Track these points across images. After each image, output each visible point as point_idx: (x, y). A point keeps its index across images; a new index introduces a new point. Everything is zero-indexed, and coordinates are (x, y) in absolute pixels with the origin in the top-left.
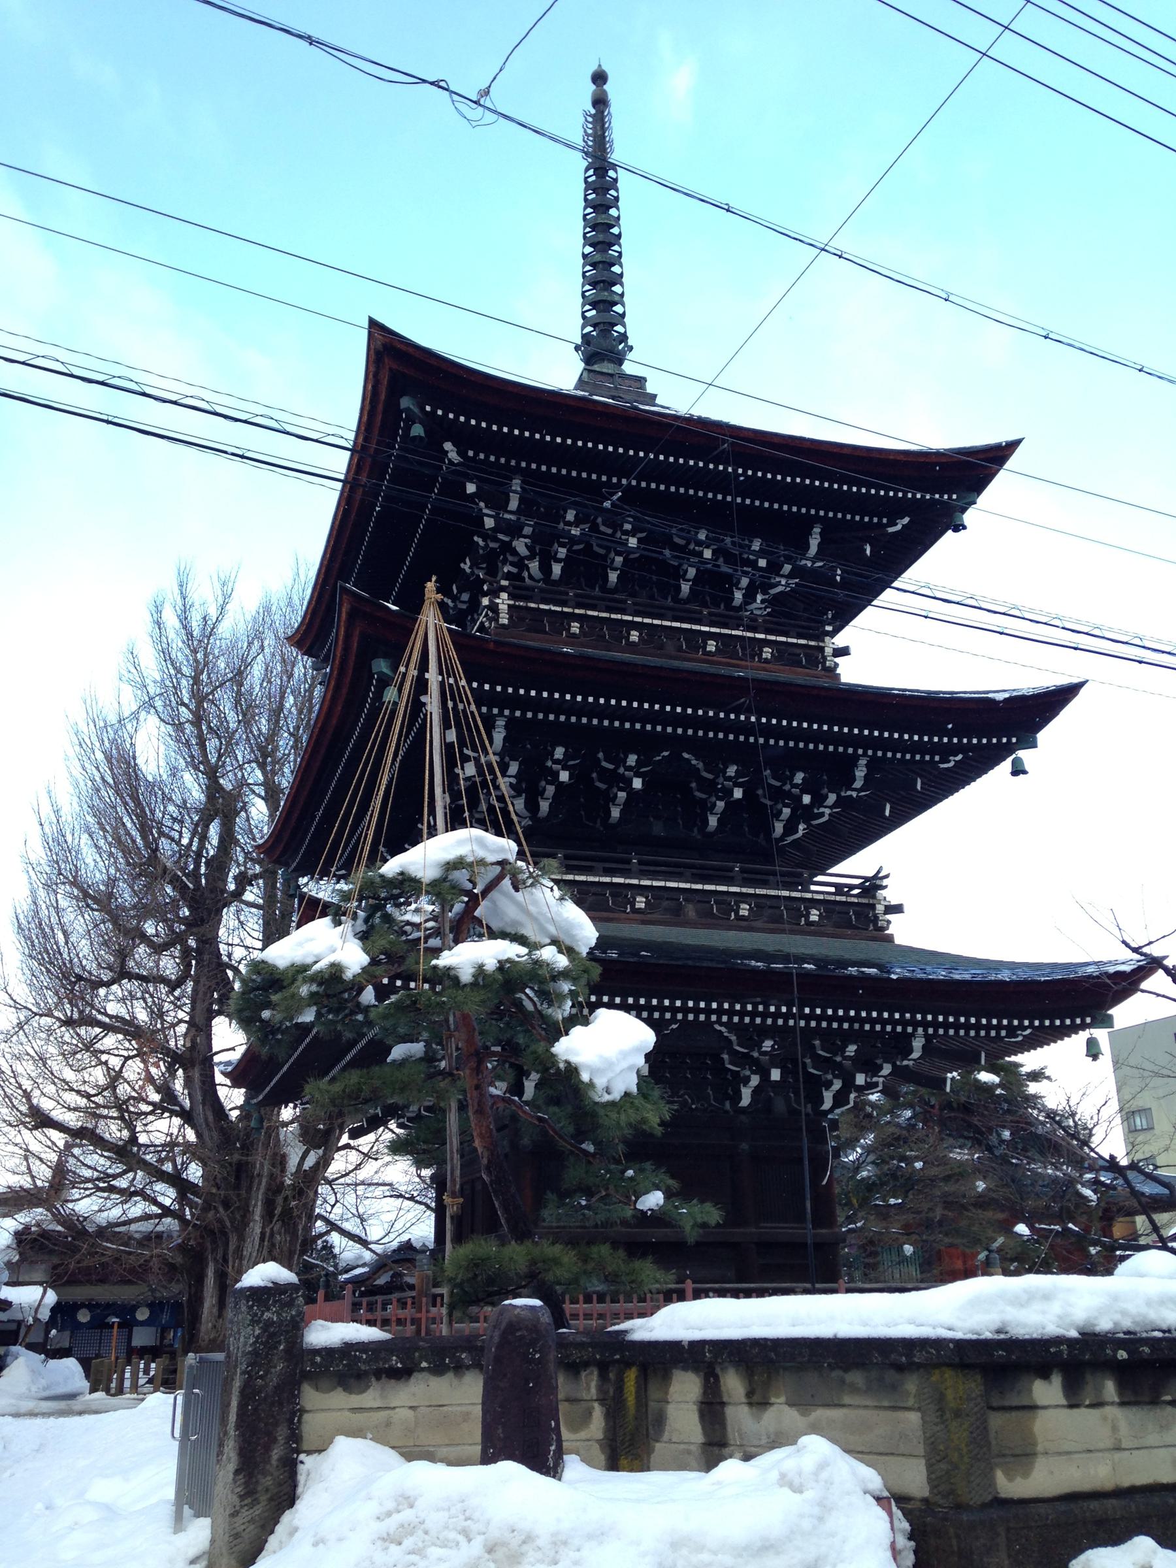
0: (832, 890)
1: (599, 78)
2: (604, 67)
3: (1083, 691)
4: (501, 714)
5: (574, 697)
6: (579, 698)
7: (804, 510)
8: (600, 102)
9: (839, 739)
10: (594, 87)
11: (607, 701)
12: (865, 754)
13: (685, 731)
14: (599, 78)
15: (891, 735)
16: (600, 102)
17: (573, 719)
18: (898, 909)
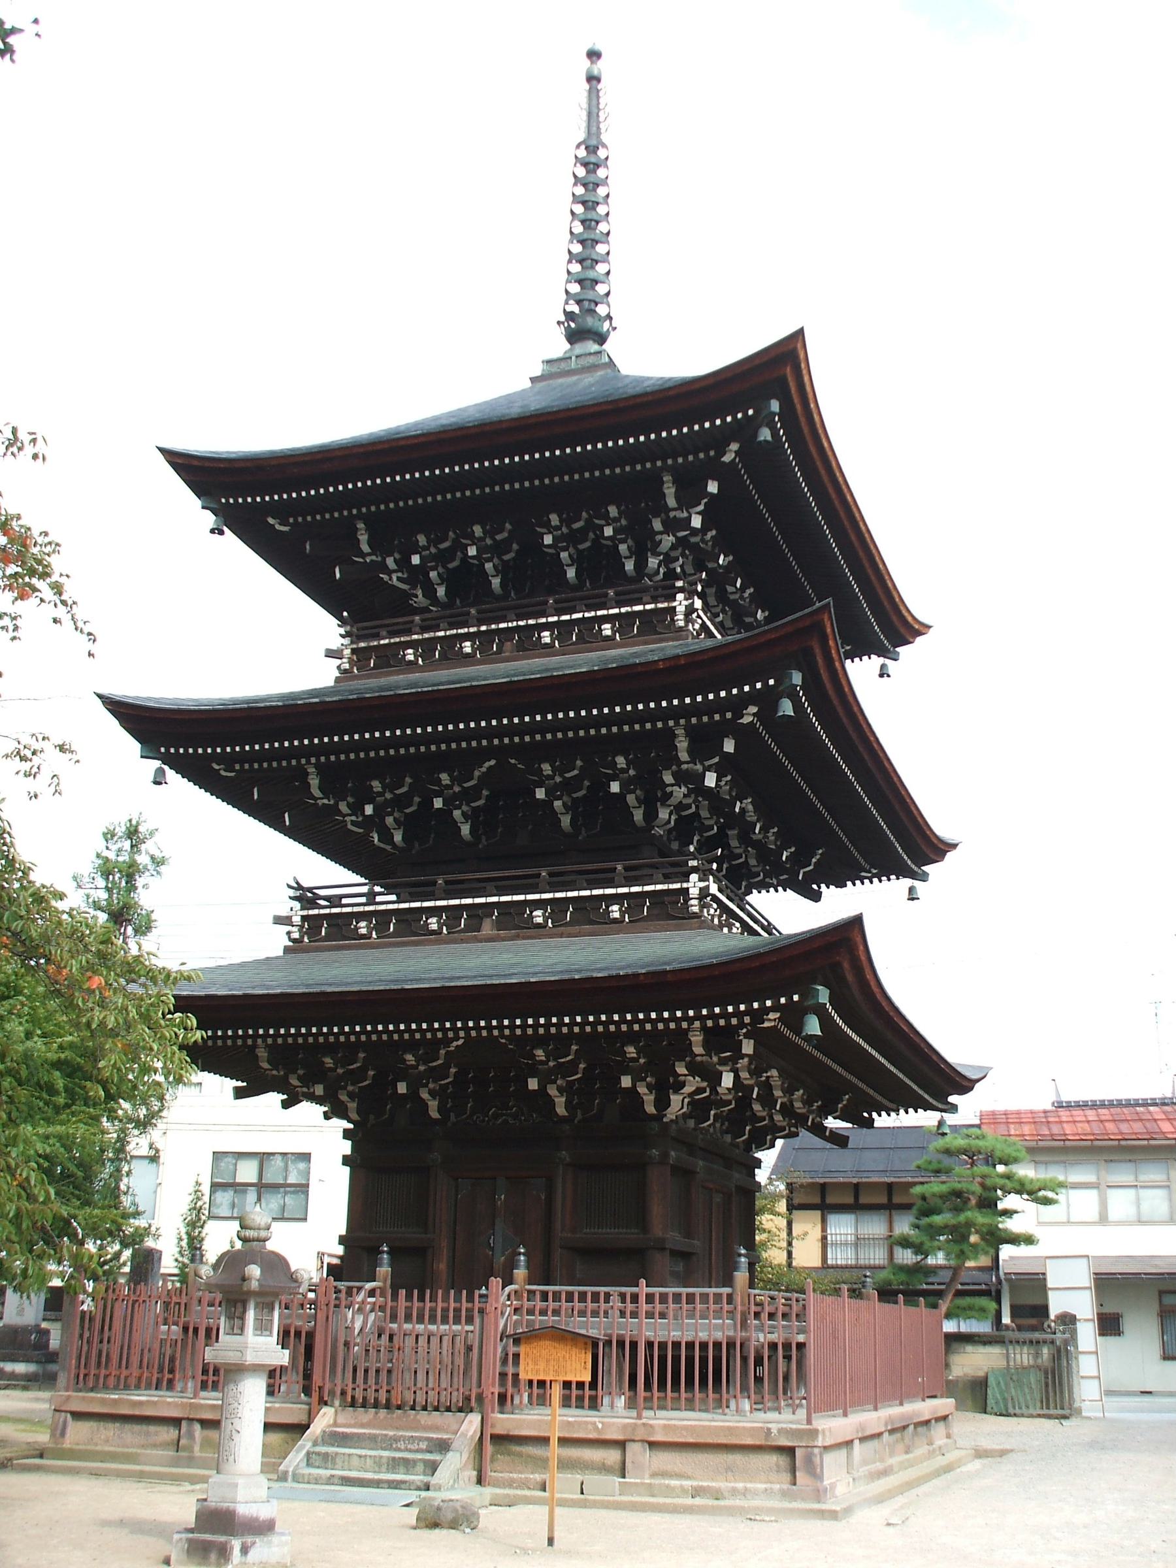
0: (363, 900)
3: (105, 691)
4: (308, 762)
6: (572, 714)
11: (670, 702)
15: (205, 751)
17: (549, 736)
18: (279, 920)
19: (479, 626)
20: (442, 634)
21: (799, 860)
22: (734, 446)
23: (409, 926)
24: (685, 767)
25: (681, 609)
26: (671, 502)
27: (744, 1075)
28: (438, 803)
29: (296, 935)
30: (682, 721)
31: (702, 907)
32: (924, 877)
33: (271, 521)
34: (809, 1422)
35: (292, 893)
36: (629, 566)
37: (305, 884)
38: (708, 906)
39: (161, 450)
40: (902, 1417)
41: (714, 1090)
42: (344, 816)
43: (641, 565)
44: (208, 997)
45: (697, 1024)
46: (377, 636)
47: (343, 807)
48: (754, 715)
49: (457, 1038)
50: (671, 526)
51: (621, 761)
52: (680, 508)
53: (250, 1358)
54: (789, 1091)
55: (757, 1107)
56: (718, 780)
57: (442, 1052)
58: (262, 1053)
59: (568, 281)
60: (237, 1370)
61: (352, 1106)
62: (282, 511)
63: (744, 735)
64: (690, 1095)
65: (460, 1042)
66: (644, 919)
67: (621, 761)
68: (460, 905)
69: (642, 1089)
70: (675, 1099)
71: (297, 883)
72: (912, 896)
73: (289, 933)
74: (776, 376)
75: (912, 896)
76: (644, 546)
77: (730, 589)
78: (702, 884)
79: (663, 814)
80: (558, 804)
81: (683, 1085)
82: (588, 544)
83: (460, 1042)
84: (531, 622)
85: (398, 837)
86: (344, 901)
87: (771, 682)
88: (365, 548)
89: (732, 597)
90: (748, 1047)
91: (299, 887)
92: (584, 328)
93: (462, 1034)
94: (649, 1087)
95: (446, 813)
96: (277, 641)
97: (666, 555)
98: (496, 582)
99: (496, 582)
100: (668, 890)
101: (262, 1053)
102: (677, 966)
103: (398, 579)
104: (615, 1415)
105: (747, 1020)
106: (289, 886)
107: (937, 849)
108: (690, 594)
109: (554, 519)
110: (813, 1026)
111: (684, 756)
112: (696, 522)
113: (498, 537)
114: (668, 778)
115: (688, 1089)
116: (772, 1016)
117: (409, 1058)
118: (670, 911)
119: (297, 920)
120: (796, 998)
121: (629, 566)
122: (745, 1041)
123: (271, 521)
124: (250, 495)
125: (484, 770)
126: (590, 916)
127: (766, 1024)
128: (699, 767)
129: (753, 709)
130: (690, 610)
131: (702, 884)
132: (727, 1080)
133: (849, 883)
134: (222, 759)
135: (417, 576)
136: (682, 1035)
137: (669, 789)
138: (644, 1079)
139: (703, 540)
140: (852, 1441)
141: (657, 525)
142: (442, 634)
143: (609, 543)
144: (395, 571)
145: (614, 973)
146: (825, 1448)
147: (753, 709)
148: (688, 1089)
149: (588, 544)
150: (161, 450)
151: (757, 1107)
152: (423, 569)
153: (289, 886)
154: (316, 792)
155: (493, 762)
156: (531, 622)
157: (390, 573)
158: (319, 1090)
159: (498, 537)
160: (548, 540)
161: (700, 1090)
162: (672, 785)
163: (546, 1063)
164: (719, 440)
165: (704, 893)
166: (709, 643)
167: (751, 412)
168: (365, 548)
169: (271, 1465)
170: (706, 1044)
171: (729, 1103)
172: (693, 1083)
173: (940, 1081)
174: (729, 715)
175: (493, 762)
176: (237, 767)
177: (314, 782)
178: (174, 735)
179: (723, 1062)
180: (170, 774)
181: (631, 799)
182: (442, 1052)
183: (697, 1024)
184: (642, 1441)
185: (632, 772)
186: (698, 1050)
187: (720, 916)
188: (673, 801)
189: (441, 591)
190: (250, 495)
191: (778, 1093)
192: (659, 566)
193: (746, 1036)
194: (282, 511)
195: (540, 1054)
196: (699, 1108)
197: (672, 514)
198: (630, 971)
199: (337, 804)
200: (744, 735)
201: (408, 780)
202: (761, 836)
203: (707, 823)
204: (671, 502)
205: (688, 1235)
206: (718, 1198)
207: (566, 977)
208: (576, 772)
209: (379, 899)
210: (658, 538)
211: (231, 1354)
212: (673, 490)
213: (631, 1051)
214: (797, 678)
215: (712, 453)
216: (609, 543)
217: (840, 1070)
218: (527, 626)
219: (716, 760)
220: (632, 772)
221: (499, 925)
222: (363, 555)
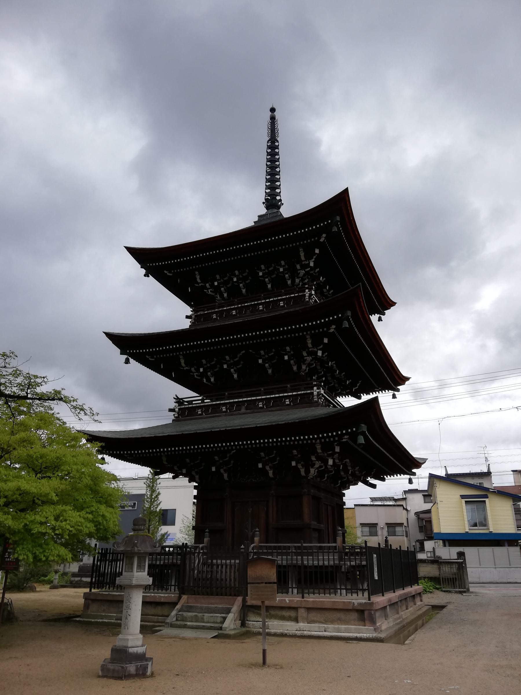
0: (200, 402)
1: (273, 110)
2: (274, 106)
3: (107, 331)
5: (237, 337)
7: (200, 266)
8: (273, 118)
9: (297, 330)
12: (307, 334)
13: (253, 342)
14: (273, 110)
16: (273, 118)
18: (187, 317)
19: (238, 305)
20: (225, 308)
21: (353, 385)
22: (324, 235)
23: (215, 410)
24: (311, 349)
25: (307, 295)
26: (303, 258)
27: (337, 461)
28: (225, 366)
29: (176, 415)
30: (309, 332)
31: (318, 399)
32: (398, 390)
33: (165, 272)
34: (369, 600)
35: (175, 400)
36: (289, 282)
37: (180, 398)
38: (321, 398)
39: (125, 247)
40: (405, 594)
41: (326, 467)
42: (193, 373)
43: (293, 282)
44: (142, 437)
45: (318, 441)
46: (204, 311)
47: (193, 369)
48: (334, 329)
49: (232, 450)
50: (303, 267)
51: (288, 348)
52: (306, 260)
53: (134, 582)
54: (353, 467)
55: (342, 473)
56: (323, 354)
57: (228, 455)
58: (164, 459)
59: (266, 189)
60: (132, 587)
61: (197, 477)
62: (169, 268)
63: (331, 336)
64: (318, 468)
65: (234, 451)
66: (298, 404)
67: (288, 348)
68: (234, 402)
69: (300, 466)
70: (312, 471)
71: (177, 396)
72: (394, 397)
73: (174, 415)
74: (340, 205)
75: (394, 397)
76: (294, 274)
77: (325, 290)
78: (318, 391)
79: (304, 367)
80: (267, 365)
81: (314, 464)
82: (275, 276)
83: (234, 451)
84: (256, 303)
85: (212, 380)
86: (194, 402)
87: (340, 315)
88: (199, 281)
89: (325, 294)
90: (337, 449)
91: (178, 398)
92: (272, 202)
93: (234, 448)
94: (302, 466)
95: (228, 371)
96: (168, 313)
97: (302, 278)
98: (244, 291)
99: (244, 291)
100: (306, 393)
101: (164, 459)
102: (309, 418)
103: (211, 291)
104: (291, 598)
105: (337, 439)
106: (174, 398)
107: (403, 380)
108: (310, 289)
109: (263, 267)
110: (361, 440)
111: (310, 345)
112: (312, 264)
113: (244, 275)
114: (305, 354)
115: (317, 466)
116: (346, 437)
117: (216, 458)
118: (307, 401)
119: (177, 410)
120: (354, 429)
121: (289, 282)
122: (336, 447)
123: (165, 272)
124: (151, 260)
125: (241, 354)
126: (278, 404)
127: (344, 440)
128: (315, 349)
129: (334, 327)
130: (311, 295)
131: (318, 391)
132: (331, 462)
133: (371, 393)
134: (149, 353)
135: (217, 289)
136: (313, 446)
137: (306, 358)
138: (300, 463)
139: (314, 272)
140: (386, 606)
141: (298, 267)
142: (225, 308)
143: (282, 275)
144: (209, 289)
145: (287, 422)
146: (376, 610)
147: (334, 327)
148: (317, 466)
149: (275, 276)
150: (125, 247)
151: (342, 473)
152: (218, 287)
153: (174, 398)
154: (183, 365)
155: (244, 352)
156: (256, 303)
157: (208, 289)
158: (184, 471)
159: (244, 275)
160: (261, 274)
161: (321, 467)
162: (306, 356)
163: (265, 457)
164: (318, 233)
165: (319, 394)
166: (335, 409)
167: (329, 221)
168: (199, 281)
169: (146, 629)
170: (322, 449)
171: (332, 471)
172: (318, 464)
173: (407, 463)
174: (325, 329)
175: (244, 352)
176: (155, 357)
177: (182, 361)
178: (135, 346)
179: (329, 456)
180: (131, 360)
181: (292, 362)
182: (228, 455)
183: (318, 441)
184: (304, 608)
185: (292, 353)
186: (319, 451)
187: (325, 403)
188: (307, 362)
189: (225, 295)
190: (151, 260)
191: (349, 468)
192: (300, 282)
193: (337, 445)
194: (169, 268)
195: (262, 454)
196: (321, 474)
197: (303, 263)
198: (292, 421)
199: (191, 369)
200: (331, 336)
201: (215, 359)
202: (339, 376)
203: (320, 371)
204: (303, 258)
205: (319, 522)
206: (329, 508)
207: (269, 424)
208: (272, 353)
209: (205, 401)
210: (299, 271)
211: (126, 580)
212: (303, 254)
213: (295, 452)
214: (349, 313)
215: (316, 238)
216: (282, 275)
217: (372, 459)
218: (254, 304)
219: (321, 347)
220: (292, 353)
221: (247, 409)
222: (198, 283)
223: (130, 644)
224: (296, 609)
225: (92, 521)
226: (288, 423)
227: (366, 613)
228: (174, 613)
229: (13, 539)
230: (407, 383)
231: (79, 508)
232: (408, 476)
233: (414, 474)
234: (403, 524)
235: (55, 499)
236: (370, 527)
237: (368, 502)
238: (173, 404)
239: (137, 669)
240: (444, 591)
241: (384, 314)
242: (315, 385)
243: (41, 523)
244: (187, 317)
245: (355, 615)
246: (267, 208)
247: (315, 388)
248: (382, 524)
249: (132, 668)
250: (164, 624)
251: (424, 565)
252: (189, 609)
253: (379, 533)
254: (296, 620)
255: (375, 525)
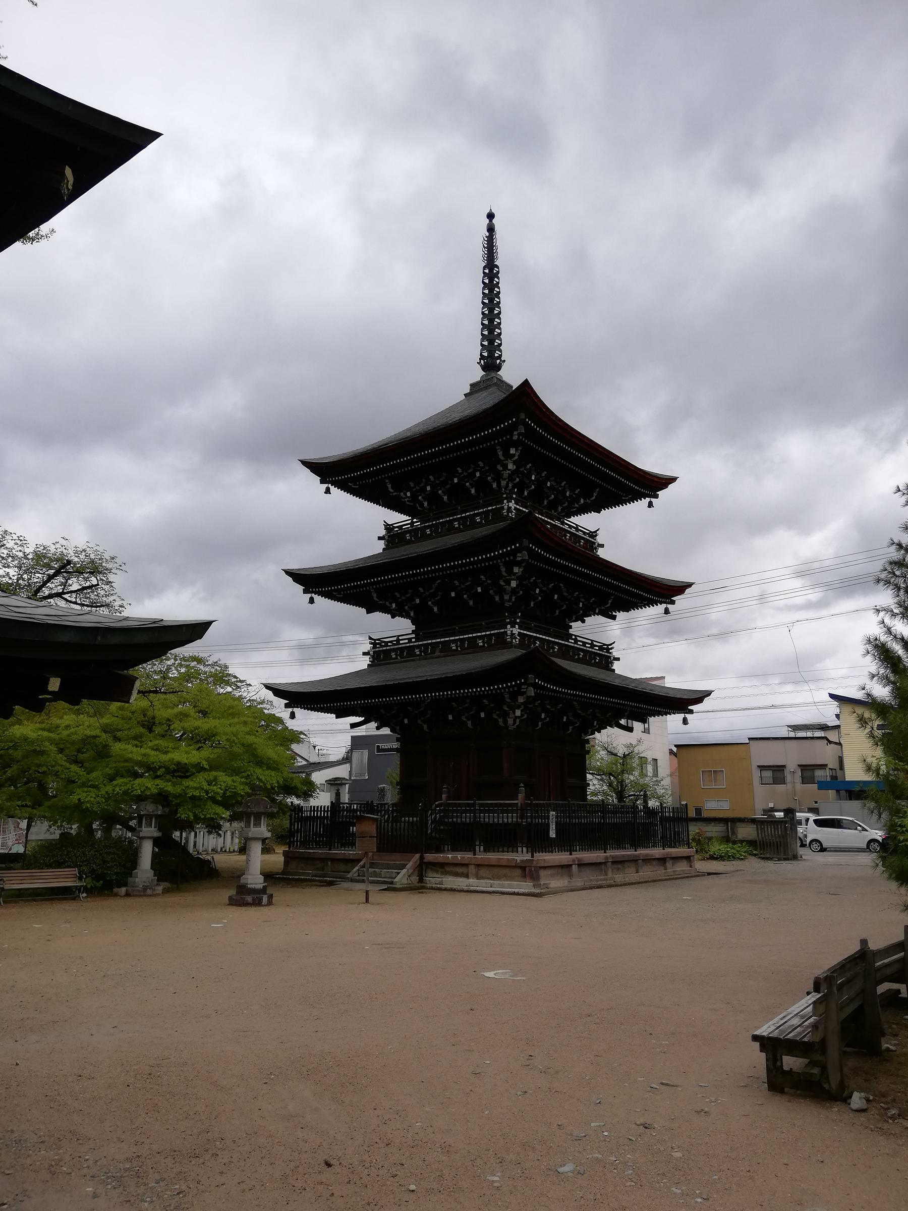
1: (491, 216)
8: (491, 229)
10: (488, 221)
14: (491, 216)
16: (491, 229)
18: (380, 538)
25: (506, 507)
32: (673, 603)
92: (491, 361)
96: (359, 528)
177: (375, 595)
180: (332, 488)
190: (336, 473)
223: (249, 882)
224: (467, 865)
225: (246, 784)
226: (447, 677)
227: (527, 869)
228: (357, 868)
229: (175, 802)
230: (687, 591)
231: (235, 772)
232: (682, 715)
233: (691, 712)
234: (826, 765)
235: (207, 767)
236: (773, 771)
237: (785, 732)
238: (383, 532)
239: (253, 900)
240: (763, 858)
241: (657, 497)
242: (509, 623)
243: (196, 788)
244: (380, 538)
245: (519, 871)
246: (484, 368)
247: (509, 626)
248: (792, 765)
249: (249, 899)
250: (345, 879)
251: (744, 825)
252: (372, 865)
253: (789, 778)
254: (467, 876)
255: (780, 768)
